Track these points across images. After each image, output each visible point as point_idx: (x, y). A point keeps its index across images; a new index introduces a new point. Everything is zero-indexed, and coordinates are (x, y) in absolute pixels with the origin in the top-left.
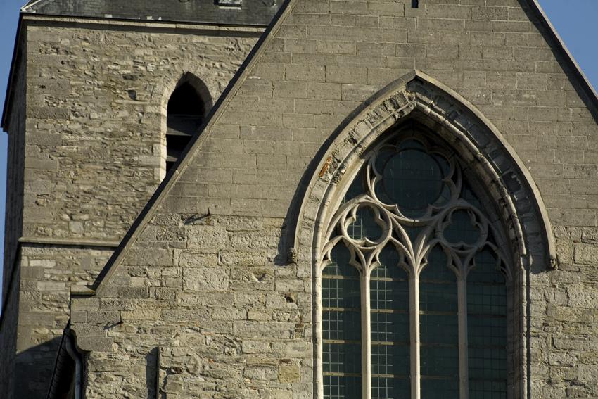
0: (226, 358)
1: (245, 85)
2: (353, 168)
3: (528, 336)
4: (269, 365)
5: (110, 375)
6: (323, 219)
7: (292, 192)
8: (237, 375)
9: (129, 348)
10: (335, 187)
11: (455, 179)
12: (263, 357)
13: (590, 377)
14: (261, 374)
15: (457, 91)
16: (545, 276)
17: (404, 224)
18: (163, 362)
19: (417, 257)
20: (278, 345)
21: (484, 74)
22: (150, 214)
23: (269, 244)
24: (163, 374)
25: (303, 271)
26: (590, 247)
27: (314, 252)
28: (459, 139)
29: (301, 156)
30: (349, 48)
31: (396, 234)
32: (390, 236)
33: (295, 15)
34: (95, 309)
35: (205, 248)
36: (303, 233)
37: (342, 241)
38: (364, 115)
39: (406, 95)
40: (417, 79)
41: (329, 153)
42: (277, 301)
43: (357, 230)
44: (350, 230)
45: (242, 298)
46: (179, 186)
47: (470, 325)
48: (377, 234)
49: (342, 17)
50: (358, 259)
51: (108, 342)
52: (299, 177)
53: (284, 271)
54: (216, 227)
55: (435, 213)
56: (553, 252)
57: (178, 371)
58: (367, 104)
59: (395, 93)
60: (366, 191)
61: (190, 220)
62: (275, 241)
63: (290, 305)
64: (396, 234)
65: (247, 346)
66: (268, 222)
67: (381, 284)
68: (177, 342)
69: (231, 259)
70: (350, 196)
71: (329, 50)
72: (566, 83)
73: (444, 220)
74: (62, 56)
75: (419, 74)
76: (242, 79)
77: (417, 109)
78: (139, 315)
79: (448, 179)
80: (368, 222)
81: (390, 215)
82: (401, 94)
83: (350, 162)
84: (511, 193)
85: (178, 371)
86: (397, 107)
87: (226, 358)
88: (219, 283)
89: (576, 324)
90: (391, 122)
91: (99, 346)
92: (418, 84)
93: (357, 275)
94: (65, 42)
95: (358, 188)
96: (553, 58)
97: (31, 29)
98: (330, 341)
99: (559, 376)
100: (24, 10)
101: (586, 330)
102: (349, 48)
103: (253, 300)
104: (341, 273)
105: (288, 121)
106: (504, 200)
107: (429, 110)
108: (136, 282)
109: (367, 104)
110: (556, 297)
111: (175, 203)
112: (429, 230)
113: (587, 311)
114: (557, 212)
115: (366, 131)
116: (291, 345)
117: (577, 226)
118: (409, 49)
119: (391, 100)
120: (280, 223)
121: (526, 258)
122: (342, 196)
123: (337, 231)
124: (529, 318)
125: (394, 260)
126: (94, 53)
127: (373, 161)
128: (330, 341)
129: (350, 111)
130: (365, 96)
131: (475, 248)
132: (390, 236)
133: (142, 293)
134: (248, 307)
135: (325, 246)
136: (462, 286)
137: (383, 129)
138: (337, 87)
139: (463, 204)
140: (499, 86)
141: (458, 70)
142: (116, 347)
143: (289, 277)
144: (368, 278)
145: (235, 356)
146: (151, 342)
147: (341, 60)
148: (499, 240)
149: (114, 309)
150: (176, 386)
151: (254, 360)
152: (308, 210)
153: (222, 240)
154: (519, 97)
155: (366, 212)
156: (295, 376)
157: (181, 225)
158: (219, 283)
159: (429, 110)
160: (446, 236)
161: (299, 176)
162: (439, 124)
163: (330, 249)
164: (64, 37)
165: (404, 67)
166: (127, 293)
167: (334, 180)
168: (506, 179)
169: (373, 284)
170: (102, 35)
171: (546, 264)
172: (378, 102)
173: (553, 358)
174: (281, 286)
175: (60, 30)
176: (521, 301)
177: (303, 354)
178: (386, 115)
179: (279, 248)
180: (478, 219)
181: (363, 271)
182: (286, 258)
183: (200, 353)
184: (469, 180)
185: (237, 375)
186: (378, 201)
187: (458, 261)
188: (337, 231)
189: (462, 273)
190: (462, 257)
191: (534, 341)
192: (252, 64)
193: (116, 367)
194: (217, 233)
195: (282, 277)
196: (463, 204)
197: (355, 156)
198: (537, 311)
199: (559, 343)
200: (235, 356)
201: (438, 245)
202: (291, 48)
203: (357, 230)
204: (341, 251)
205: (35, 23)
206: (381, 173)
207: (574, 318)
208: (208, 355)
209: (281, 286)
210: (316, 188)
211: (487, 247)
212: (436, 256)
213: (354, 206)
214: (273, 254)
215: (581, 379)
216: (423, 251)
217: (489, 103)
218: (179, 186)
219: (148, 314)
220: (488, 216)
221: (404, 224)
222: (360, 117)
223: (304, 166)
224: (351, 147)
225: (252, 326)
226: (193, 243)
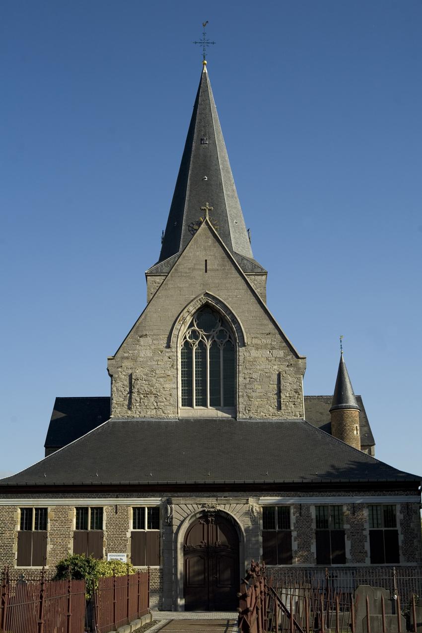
0: (151, 375)
1: (157, 297)
3: (239, 366)
5: (118, 381)
7: (170, 327)
9: (124, 373)
11: (219, 321)
12: (162, 375)
13: (256, 376)
16: (244, 348)
17: (204, 335)
18: (133, 377)
20: (166, 371)
21: (226, 291)
22: (129, 335)
23: (164, 343)
24: (133, 380)
26: (256, 339)
27: (177, 344)
28: (219, 309)
29: (173, 316)
30: (187, 285)
31: (202, 338)
33: (171, 276)
34: (114, 363)
36: (173, 339)
38: (191, 304)
39: (204, 298)
40: (207, 293)
41: (181, 315)
42: (166, 359)
43: (191, 337)
44: (189, 337)
45: (156, 358)
46: (138, 327)
47: (224, 363)
48: (196, 338)
49: (185, 276)
50: (191, 345)
51: (118, 372)
53: (168, 350)
54: (149, 338)
55: (214, 331)
56: (246, 341)
57: (138, 380)
58: (192, 301)
59: (200, 297)
62: (165, 342)
63: (170, 360)
64: (202, 338)
65: (158, 372)
66: (163, 336)
67: (198, 352)
69: (153, 347)
70: (189, 328)
71: (181, 286)
72: (250, 292)
73: (217, 333)
76: (156, 296)
77: (207, 302)
79: (218, 321)
80: (194, 335)
81: (200, 332)
82: (202, 298)
84: (234, 325)
85: (138, 380)
86: (201, 301)
87: (151, 375)
88: (149, 354)
89: (252, 362)
90: (199, 306)
91: (115, 373)
92: (207, 294)
95: (191, 325)
96: (246, 285)
97: (148, 277)
98: (183, 369)
99: (247, 377)
100: (146, 272)
102: (187, 285)
103: (159, 359)
104: (187, 350)
105: (169, 307)
106: (232, 327)
107: (210, 302)
108: (126, 355)
109: (192, 301)
110: (247, 354)
111: (136, 332)
112: (212, 337)
113: (255, 358)
114: (247, 330)
115: (192, 309)
116: (170, 371)
117: (253, 333)
118: (205, 285)
119: (199, 300)
120: (167, 336)
121: (238, 343)
122: (187, 328)
123: (185, 338)
124: (239, 360)
125: (202, 345)
127: (196, 317)
128: (183, 369)
129: (187, 303)
130: (192, 299)
131: (225, 341)
132: (200, 338)
133: (127, 358)
134: (158, 361)
135: (181, 342)
137: (197, 308)
138: (184, 297)
139: (222, 328)
140: (231, 294)
141: (218, 290)
142: (120, 373)
143: (169, 352)
144: (194, 351)
145: (154, 375)
146: (130, 372)
147: (184, 289)
148: (232, 338)
149: (120, 363)
151: (159, 376)
152: (175, 332)
153: (150, 342)
154: (236, 296)
155: (194, 332)
157: (138, 338)
158: (149, 354)
159: (210, 302)
160: (226, 338)
161: (173, 322)
162: (214, 306)
163: (183, 343)
166: (123, 358)
167: (183, 323)
168: (233, 321)
169: (196, 353)
171: (244, 345)
174: (167, 355)
176: (237, 356)
177: (174, 374)
178: (198, 304)
179: (167, 343)
180: (226, 332)
181: (193, 349)
183: (144, 374)
184: (223, 320)
185: (155, 380)
186: (197, 329)
187: (220, 344)
188: (185, 338)
189: (221, 348)
190: (222, 344)
191: (240, 367)
192: (159, 291)
193: (120, 379)
196: (222, 328)
198: (241, 358)
200: (154, 375)
202: (170, 286)
203: (191, 337)
204: (187, 343)
205: (149, 276)
206: (198, 320)
207: (252, 360)
208: (147, 375)
209: (167, 355)
210: (177, 326)
211: (229, 340)
212: (214, 345)
213: (190, 330)
214: (165, 345)
215: (253, 377)
216: (210, 342)
217: (228, 299)
218: (138, 327)
219: (129, 364)
220: (229, 332)
221: (204, 335)
222: (190, 305)
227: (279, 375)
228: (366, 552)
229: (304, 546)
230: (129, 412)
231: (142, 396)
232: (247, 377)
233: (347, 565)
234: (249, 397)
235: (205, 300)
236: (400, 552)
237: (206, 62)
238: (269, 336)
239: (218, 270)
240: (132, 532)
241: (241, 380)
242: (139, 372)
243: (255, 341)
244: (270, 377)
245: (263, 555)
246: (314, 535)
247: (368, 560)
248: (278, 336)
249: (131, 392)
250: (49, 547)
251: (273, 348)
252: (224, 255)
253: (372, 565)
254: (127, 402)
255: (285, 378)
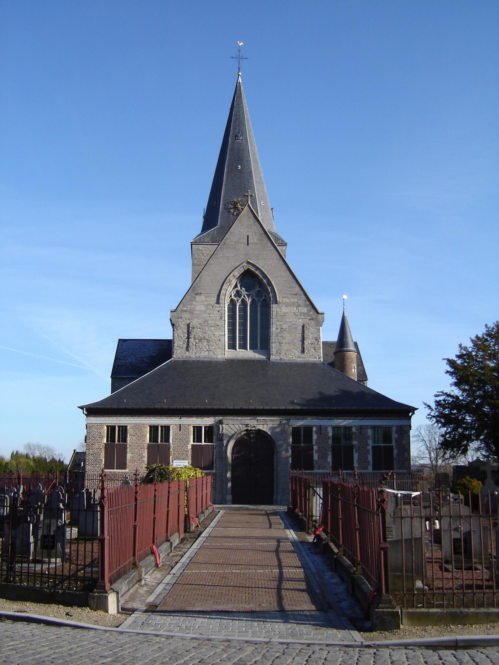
2: (234, 282)
4: (214, 326)
6: (227, 294)
8: (207, 328)
10: (229, 287)
11: (258, 284)
12: (213, 325)
14: (212, 328)
15: (258, 264)
16: (276, 305)
18: (191, 326)
19: (249, 301)
20: (216, 322)
24: (190, 328)
25: (222, 305)
31: (244, 296)
32: (243, 297)
35: (200, 301)
36: (222, 297)
37: (232, 299)
39: (246, 265)
40: (248, 262)
42: (216, 312)
44: (234, 296)
45: (208, 312)
48: (240, 296)
50: (235, 302)
52: (221, 284)
53: (218, 305)
55: (253, 291)
56: (278, 300)
58: (237, 267)
60: (237, 287)
61: (196, 294)
62: (216, 299)
64: (244, 296)
65: (209, 322)
68: (194, 322)
69: (206, 303)
70: (234, 288)
74: (200, 252)
75: (249, 261)
76: (208, 263)
77: (248, 268)
78: (186, 316)
79: (256, 284)
83: (233, 281)
85: (194, 328)
88: (203, 308)
90: (242, 272)
92: (248, 263)
93: (235, 306)
94: (201, 248)
95: (236, 286)
97: (193, 246)
99: (279, 327)
101: (285, 317)
108: (185, 309)
109: (237, 267)
110: (278, 310)
111: (193, 291)
112: (251, 296)
120: (217, 295)
123: (231, 296)
125: (244, 302)
126: (207, 251)
127: (239, 280)
129: (233, 269)
132: (243, 297)
134: (210, 314)
136: (259, 308)
137: (241, 273)
139: (259, 289)
142: (180, 323)
146: (188, 322)
150: (193, 331)
152: (223, 291)
153: (204, 299)
156: (220, 329)
158: (203, 308)
163: (229, 301)
164: (200, 247)
165: (245, 259)
166: (182, 311)
168: (268, 283)
169: (239, 308)
170: (209, 246)
171: (276, 302)
172: (240, 267)
173: (278, 323)
175: (200, 245)
182: (218, 302)
183: (199, 324)
185: (207, 328)
188: (231, 296)
189: (259, 305)
190: (259, 301)
191: (273, 320)
194: (203, 297)
195: (217, 307)
196: (259, 289)
197: (234, 280)
198: (274, 313)
199: (279, 320)
201: (254, 299)
202: (219, 255)
204: (232, 301)
207: (283, 314)
209: (217, 309)
211: (264, 299)
213: (235, 290)
214: (215, 302)
216: (250, 300)
221: (246, 294)
223: (222, 282)
224: (233, 277)
225: (210, 318)
226: (198, 300)
227: (303, 327)
228: (369, 462)
229: (323, 456)
230: (187, 353)
231: (197, 341)
232: (279, 327)
233: (314, 471)
234: (280, 343)
235: (246, 266)
236: (395, 462)
237: (240, 74)
238: (296, 296)
239: (257, 244)
240: (192, 445)
241: (273, 329)
242: (194, 323)
243: (285, 300)
244: (296, 328)
245: (291, 463)
246: (330, 449)
247: (370, 468)
248: (303, 297)
249: (188, 338)
250: (129, 456)
251: (299, 306)
252: (262, 232)
253: (373, 471)
254: (185, 345)
255: (308, 329)
